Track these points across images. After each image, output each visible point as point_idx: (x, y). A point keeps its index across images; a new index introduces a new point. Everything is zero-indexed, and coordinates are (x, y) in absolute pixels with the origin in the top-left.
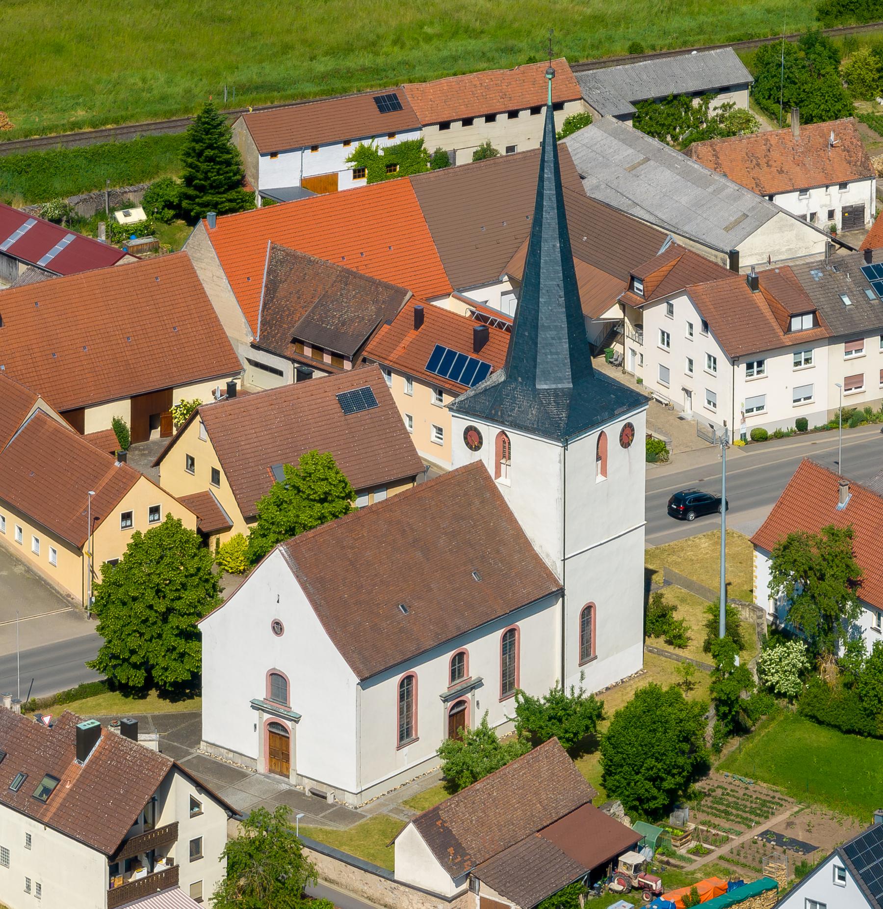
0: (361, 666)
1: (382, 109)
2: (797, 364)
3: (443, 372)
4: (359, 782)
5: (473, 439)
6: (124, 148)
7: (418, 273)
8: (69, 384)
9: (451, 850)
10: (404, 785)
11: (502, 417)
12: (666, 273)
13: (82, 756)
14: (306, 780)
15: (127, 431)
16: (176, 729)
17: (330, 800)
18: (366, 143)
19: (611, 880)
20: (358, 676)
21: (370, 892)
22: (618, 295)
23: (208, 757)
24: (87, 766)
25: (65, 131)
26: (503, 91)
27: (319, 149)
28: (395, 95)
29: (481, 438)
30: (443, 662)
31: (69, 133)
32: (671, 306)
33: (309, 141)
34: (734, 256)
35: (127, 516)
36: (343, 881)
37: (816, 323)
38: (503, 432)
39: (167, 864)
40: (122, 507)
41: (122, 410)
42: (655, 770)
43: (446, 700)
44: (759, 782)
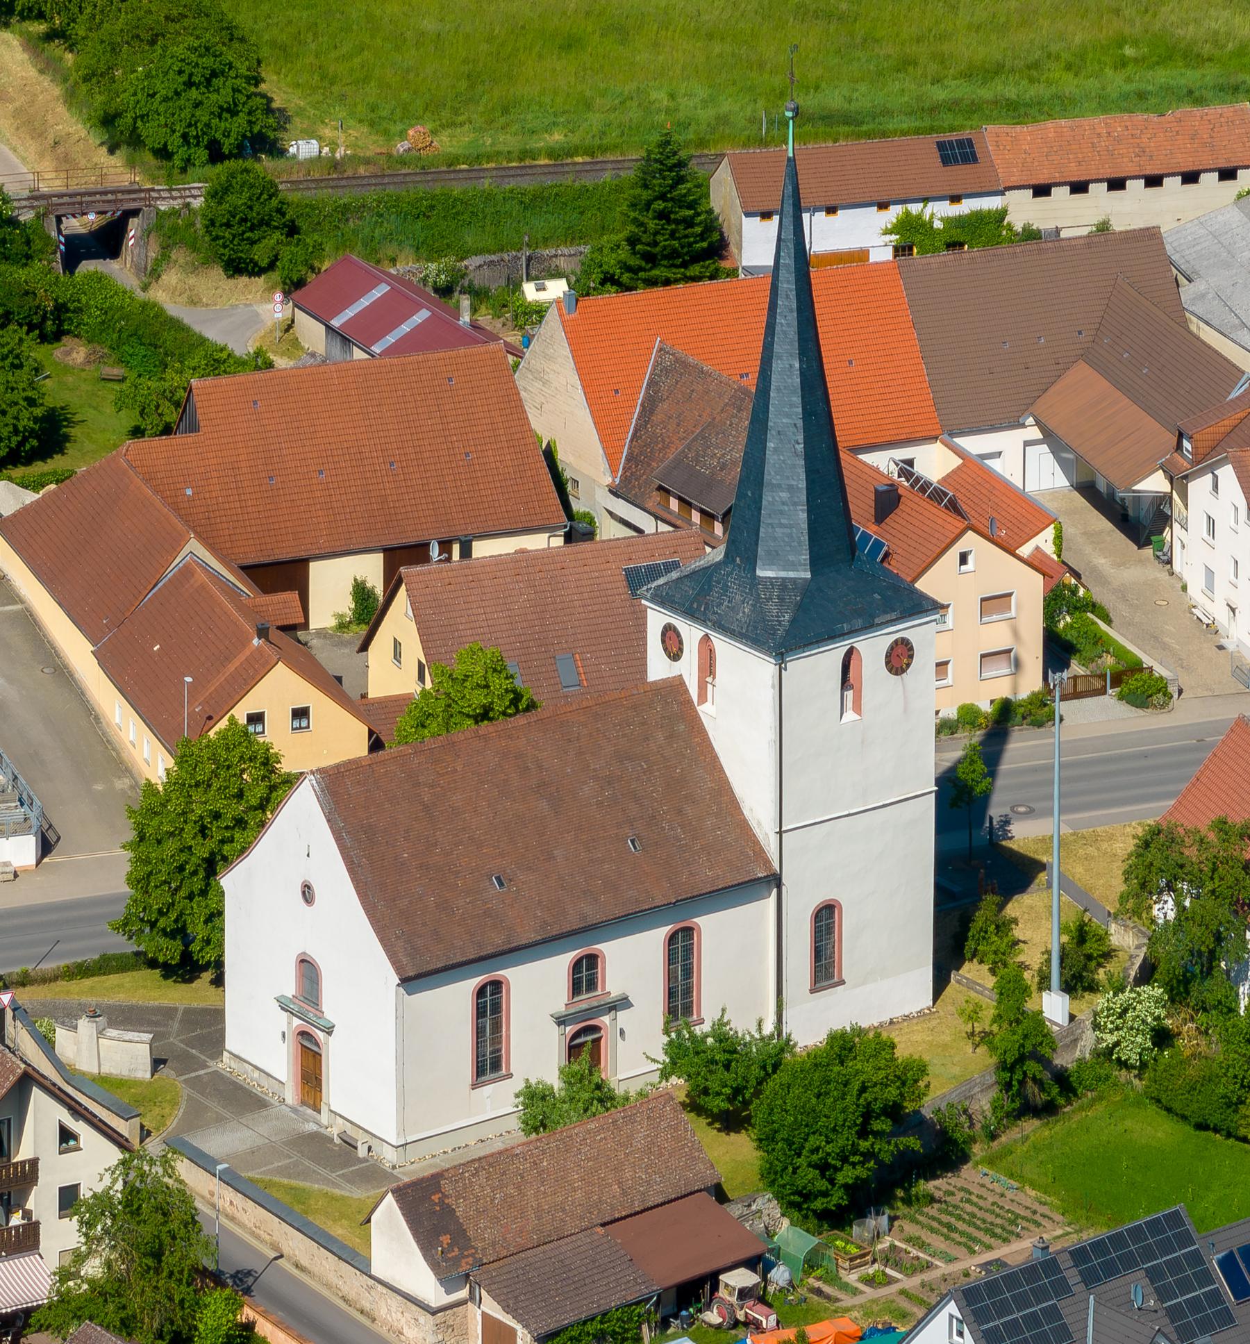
0: (405, 960)
1: (946, 160)
4: (402, 1128)
7: (890, 402)
8: (288, 524)
9: (446, 1239)
12: (1229, 429)
14: (340, 1121)
15: (376, 600)
16: (208, 1030)
17: (362, 1152)
18: (915, 208)
19: (708, 1307)
21: (344, 1289)
22: (1163, 457)
23: (228, 1075)
25: (510, 161)
26: (1142, 145)
27: (839, 212)
28: (970, 141)
30: (558, 967)
31: (514, 164)
32: (1216, 477)
33: (823, 199)
36: (315, 1269)
38: (707, 635)
39: (23, 1218)
42: (821, 1154)
43: (561, 1021)
44: (1027, 1188)
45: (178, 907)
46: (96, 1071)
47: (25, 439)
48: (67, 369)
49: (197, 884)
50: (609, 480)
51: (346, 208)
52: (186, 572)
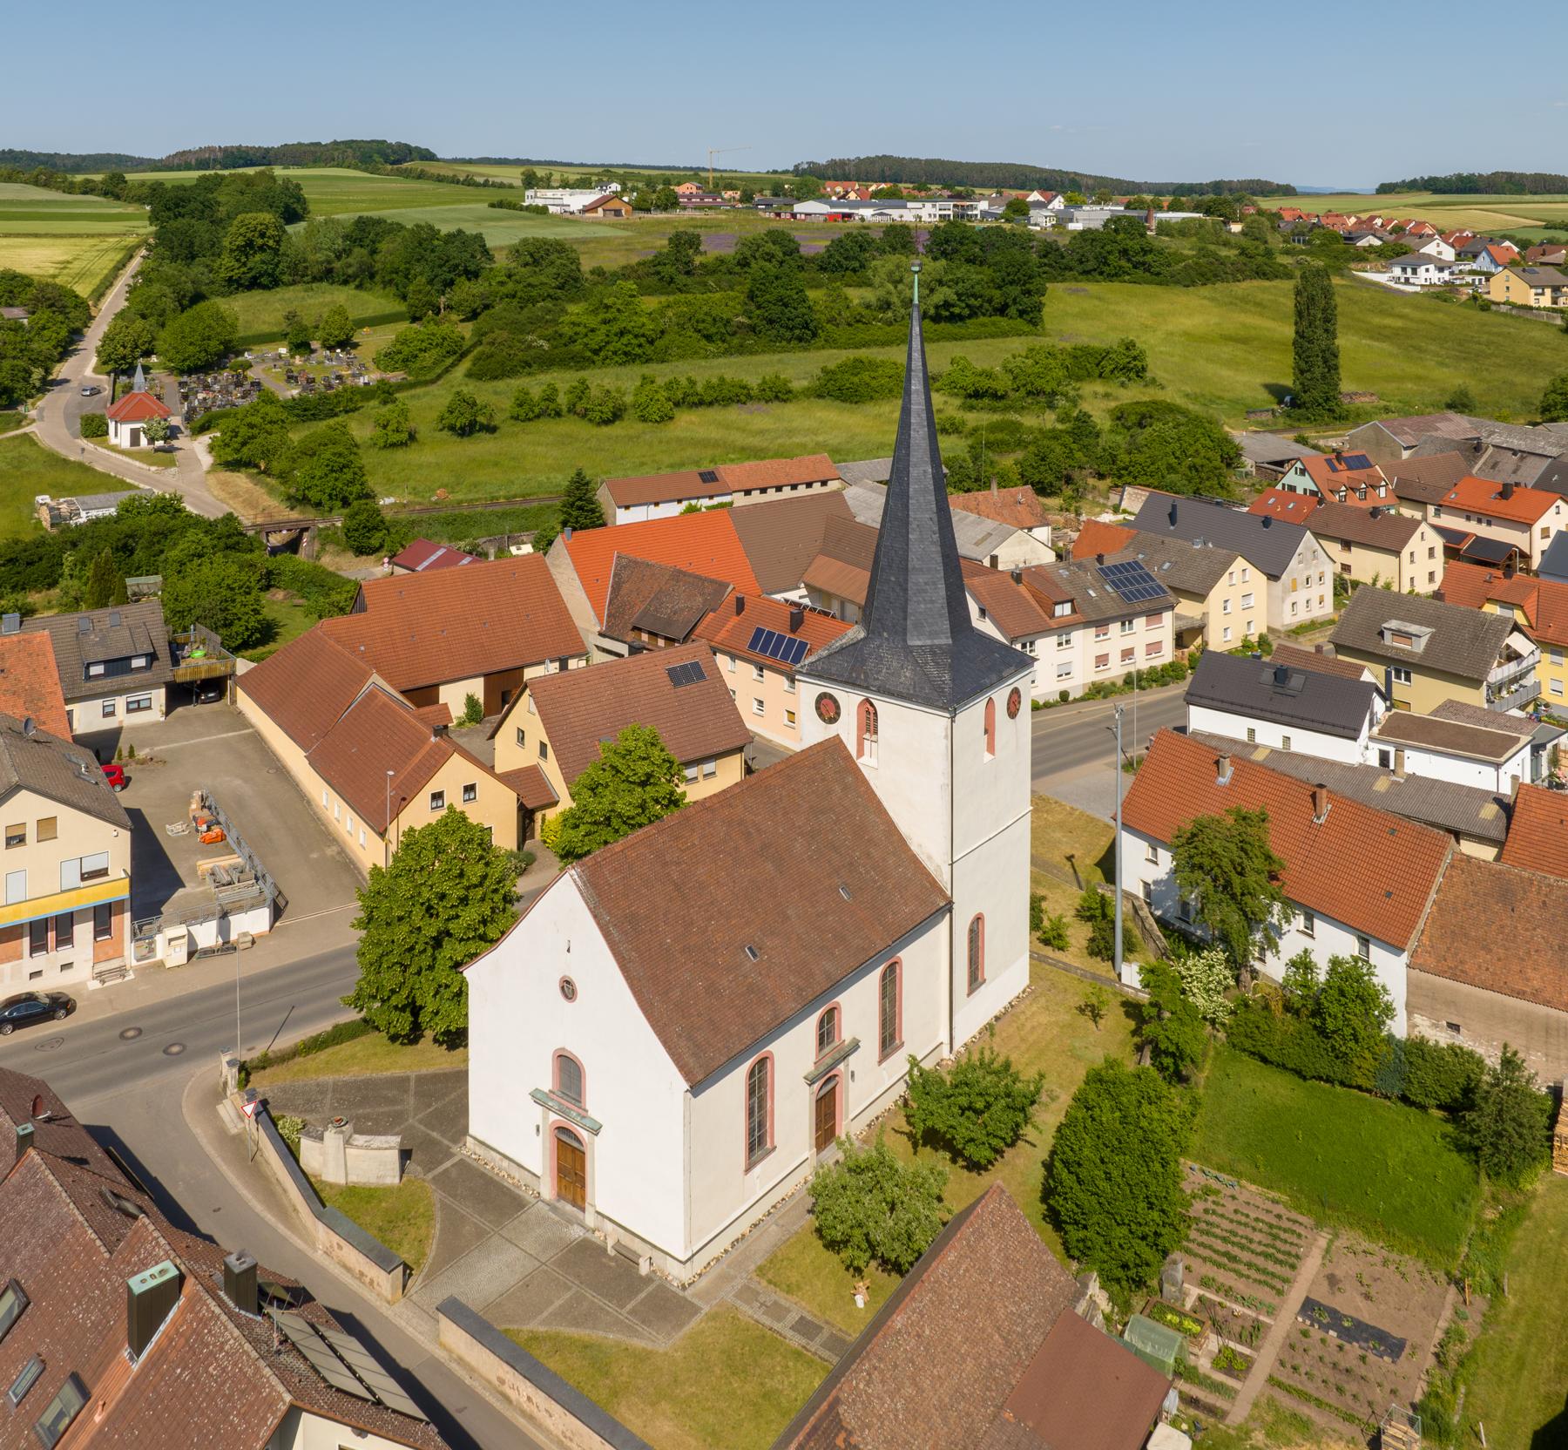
0: (691, 1062)
2: (1060, 644)
3: (764, 650)
5: (827, 709)
6: (526, 510)
10: (755, 1225)
11: (866, 680)
13: (138, 1344)
14: (609, 1226)
17: (644, 1269)
18: (693, 502)
20: (687, 1080)
23: (475, 1164)
24: (145, 1365)
29: (838, 707)
34: (994, 559)
35: (437, 796)
37: (1074, 610)
38: (867, 700)
40: (432, 787)
41: (477, 687)
45: (409, 984)
46: (343, 1182)
47: (252, 634)
48: (274, 603)
49: (425, 961)
50: (598, 629)
51: (413, 522)
52: (371, 696)
